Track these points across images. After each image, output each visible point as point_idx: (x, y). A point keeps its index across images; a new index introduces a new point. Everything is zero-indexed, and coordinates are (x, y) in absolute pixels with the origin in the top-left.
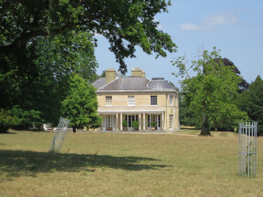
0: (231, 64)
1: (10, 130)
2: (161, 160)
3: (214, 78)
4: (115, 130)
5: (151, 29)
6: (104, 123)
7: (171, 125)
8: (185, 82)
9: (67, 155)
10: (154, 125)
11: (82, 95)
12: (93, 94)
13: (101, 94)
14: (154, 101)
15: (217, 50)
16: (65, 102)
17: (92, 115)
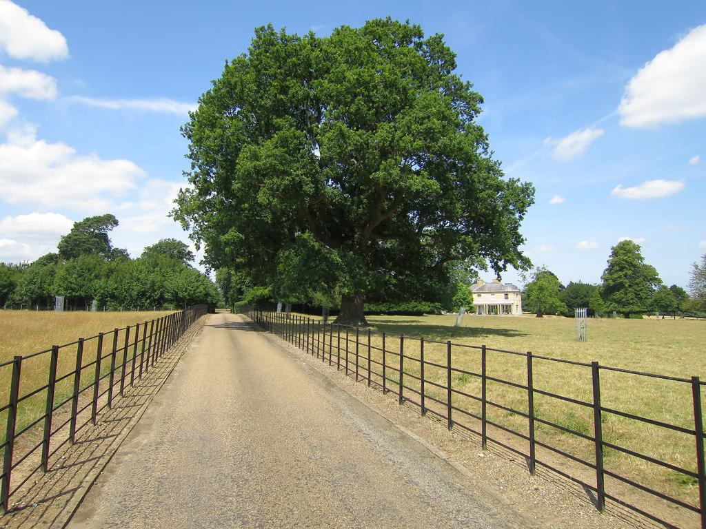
0: (553, 274)
1: (425, 315)
2: (577, 340)
3: (544, 283)
4: (484, 314)
5: (519, 255)
6: (477, 310)
7: (517, 311)
8: (526, 286)
9: (466, 328)
10: (507, 311)
11: (464, 294)
12: (470, 293)
13: (474, 293)
14: (506, 297)
15: (545, 266)
16: (454, 298)
17: (471, 305)
